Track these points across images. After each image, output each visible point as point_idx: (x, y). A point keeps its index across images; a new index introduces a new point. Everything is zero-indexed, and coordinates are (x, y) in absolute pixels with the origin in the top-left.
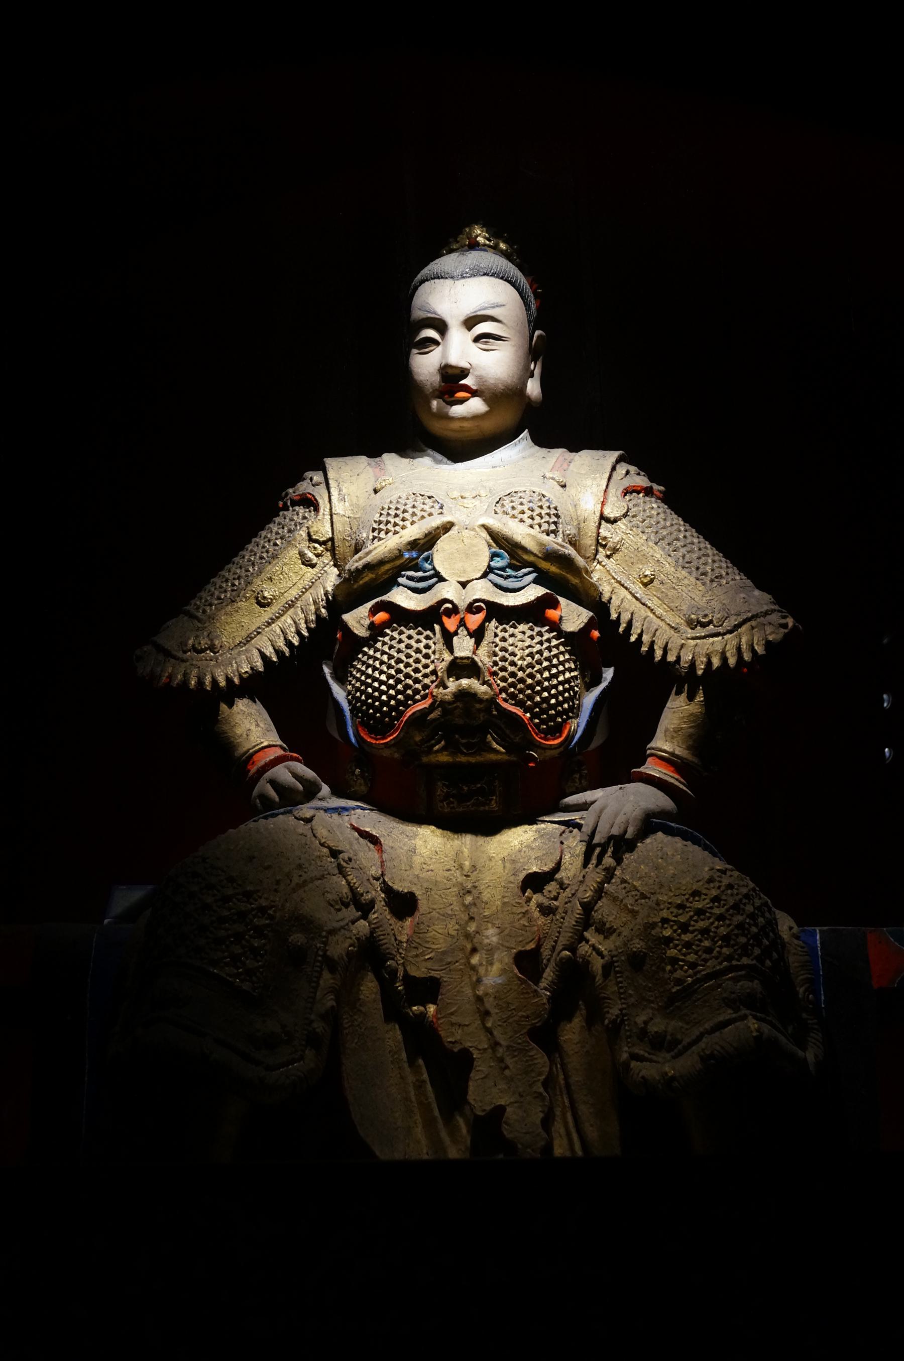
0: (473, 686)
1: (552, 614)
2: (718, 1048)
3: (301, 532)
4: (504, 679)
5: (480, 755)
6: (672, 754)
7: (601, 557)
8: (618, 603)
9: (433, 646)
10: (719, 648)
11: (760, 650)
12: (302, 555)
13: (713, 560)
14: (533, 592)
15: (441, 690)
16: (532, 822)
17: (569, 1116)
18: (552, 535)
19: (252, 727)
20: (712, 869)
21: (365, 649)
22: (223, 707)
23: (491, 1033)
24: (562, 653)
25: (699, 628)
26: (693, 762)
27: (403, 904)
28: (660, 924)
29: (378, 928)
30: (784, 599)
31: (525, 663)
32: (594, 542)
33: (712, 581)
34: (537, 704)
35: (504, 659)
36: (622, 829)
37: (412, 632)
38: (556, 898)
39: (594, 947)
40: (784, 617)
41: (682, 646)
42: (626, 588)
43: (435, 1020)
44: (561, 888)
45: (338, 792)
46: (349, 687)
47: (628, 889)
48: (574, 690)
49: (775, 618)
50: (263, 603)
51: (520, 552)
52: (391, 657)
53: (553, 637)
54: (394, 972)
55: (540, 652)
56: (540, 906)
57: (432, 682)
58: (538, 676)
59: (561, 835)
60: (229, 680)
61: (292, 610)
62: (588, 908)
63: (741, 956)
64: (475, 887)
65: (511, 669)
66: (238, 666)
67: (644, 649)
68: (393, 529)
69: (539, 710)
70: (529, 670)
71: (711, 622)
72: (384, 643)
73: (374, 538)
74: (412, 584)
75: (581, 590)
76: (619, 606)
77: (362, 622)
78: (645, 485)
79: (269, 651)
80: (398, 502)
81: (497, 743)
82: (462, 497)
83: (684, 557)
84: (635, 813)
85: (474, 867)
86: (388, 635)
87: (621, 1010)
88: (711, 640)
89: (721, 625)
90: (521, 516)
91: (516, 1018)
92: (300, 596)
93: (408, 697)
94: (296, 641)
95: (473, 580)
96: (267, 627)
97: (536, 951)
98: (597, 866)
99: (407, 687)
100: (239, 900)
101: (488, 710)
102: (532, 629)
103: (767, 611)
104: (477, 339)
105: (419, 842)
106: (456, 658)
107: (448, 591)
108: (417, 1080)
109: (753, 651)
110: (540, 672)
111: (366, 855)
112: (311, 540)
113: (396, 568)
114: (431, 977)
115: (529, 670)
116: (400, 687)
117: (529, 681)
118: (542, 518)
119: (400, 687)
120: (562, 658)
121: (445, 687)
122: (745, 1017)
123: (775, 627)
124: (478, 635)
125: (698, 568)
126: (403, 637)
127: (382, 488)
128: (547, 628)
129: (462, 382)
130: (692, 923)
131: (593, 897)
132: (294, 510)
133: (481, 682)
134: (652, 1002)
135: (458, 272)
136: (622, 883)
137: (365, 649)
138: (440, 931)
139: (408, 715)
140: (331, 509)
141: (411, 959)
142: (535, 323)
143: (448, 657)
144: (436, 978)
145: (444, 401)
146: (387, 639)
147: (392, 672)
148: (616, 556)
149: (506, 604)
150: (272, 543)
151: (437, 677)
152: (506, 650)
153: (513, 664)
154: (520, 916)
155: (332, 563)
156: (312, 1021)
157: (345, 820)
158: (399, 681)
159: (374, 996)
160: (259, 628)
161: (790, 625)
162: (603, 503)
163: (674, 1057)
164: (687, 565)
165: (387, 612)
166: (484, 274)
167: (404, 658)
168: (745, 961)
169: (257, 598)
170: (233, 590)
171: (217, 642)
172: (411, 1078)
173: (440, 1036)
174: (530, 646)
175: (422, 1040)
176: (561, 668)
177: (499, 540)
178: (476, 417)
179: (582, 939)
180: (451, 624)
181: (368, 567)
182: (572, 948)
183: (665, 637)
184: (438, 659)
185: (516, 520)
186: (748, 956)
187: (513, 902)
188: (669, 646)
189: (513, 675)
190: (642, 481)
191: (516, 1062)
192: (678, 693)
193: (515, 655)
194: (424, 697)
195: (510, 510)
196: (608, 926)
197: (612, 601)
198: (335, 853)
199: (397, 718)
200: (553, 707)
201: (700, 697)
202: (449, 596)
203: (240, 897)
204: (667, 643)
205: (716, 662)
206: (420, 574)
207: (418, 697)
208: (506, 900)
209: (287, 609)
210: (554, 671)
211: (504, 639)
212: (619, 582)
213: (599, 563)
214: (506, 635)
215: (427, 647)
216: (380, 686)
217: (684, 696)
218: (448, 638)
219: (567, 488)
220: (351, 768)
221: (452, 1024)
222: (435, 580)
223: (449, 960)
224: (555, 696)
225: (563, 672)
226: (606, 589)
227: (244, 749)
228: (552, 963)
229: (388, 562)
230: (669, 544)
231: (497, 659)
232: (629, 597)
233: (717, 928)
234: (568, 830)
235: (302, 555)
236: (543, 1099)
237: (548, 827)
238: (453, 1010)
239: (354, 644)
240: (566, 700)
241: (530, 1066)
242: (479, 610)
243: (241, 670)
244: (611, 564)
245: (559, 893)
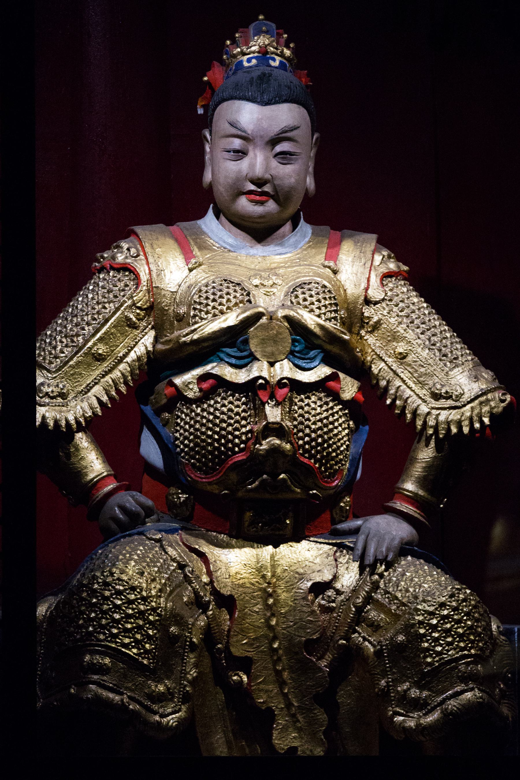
2: (455, 709)
14: (321, 372)
26: (427, 499)
27: (227, 602)
35: (301, 423)
38: (333, 601)
40: (503, 394)
44: (337, 594)
52: (216, 417)
62: (360, 610)
74: (233, 361)
104: (276, 156)
109: (482, 422)
114: (246, 656)
123: (499, 400)
130: (440, 625)
134: (410, 678)
144: (249, 657)
153: (308, 426)
183: (415, 405)
193: (310, 420)
203: (139, 601)
222: (249, 359)
233: (456, 629)
242: (284, 385)
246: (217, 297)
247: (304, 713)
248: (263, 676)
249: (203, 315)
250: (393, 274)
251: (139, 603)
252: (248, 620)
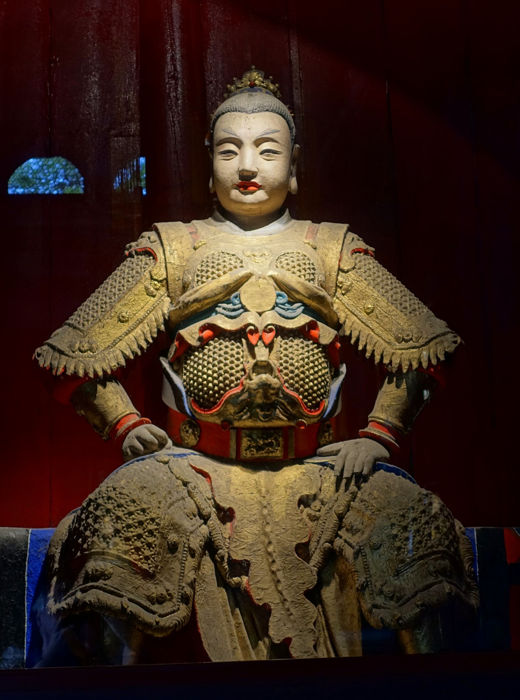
0: (269, 379)
1: (314, 332)
3: (145, 273)
4: (286, 375)
5: (271, 421)
6: (387, 421)
7: (338, 294)
8: (350, 324)
9: (242, 353)
10: (416, 356)
11: (442, 358)
12: (147, 289)
13: (411, 300)
14: (304, 320)
15: (248, 381)
16: (302, 463)
17: (329, 643)
18: (312, 282)
19: (116, 401)
20: (420, 494)
21: (196, 353)
22: (100, 387)
23: (281, 594)
24: (320, 358)
25: (403, 342)
26: (399, 426)
28: (390, 527)
29: (214, 530)
30: (454, 326)
31: (300, 364)
32: (334, 285)
33: (410, 313)
34: (306, 390)
35: (286, 362)
36: (361, 468)
37: (228, 343)
38: (319, 511)
39: (346, 541)
40: (455, 337)
41: (393, 354)
42: (355, 315)
43: (247, 586)
45: (178, 443)
46: (185, 377)
47: (367, 506)
48: (326, 381)
49: (450, 336)
50: (122, 320)
51: (294, 293)
53: (315, 348)
54: (222, 558)
55: (308, 357)
56: (309, 515)
57: (242, 376)
58: (307, 372)
59: (320, 471)
60: (104, 372)
61: (141, 324)
62: (341, 517)
63: (438, 545)
64: (269, 504)
65: (291, 368)
66: (109, 361)
67: (368, 355)
68: (211, 276)
69: (307, 394)
70: (302, 369)
71: (411, 339)
72: (209, 350)
73: (198, 281)
75: (328, 316)
76: (351, 327)
77: (194, 336)
78: (364, 248)
79: (128, 353)
80: (213, 258)
81: (282, 415)
82: (253, 255)
83: (392, 296)
84: (368, 458)
85: (268, 492)
86: (212, 345)
87: (366, 578)
88: (412, 350)
89: (418, 342)
90: (293, 269)
91: (297, 584)
92: (146, 316)
93: (226, 385)
94: (145, 346)
95: (265, 311)
96: (125, 336)
97: (307, 544)
98: (346, 491)
99: (226, 379)
100: (138, 514)
101: (277, 394)
102: (302, 343)
103: (445, 332)
104: (262, 153)
105: (232, 476)
106: (257, 361)
107: (250, 318)
108: (236, 623)
109: (438, 358)
110: (308, 370)
111: (202, 484)
112: (152, 278)
113: (215, 301)
115: (302, 369)
116: (221, 378)
117: (302, 376)
118: (305, 271)
119: (221, 378)
120: (320, 361)
121: (251, 379)
122: (441, 581)
123: (450, 342)
124: (270, 346)
125: (401, 304)
126: (222, 346)
127: (200, 246)
128: (311, 342)
129: (253, 180)
131: (344, 510)
132: (138, 258)
133: (273, 376)
135: (250, 108)
136: (362, 501)
137: (196, 353)
138: (249, 531)
139: (227, 396)
140: (165, 259)
141: (233, 549)
142: (295, 141)
143: (252, 362)
145: (240, 191)
146: (211, 347)
147: (216, 369)
148: (349, 294)
149: (287, 327)
150: (125, 280)
151: (245, 373)
152: (287, 356)
153: (292, 365)
154: (298, 522)
155: (166, 294)
156: (184, 587)
157: (184, 462)
158: (221, 375)
159: (211, 572)
160: (120, 336)
161: (459, 341)
162: (340, 261)
163: (400, 606)
164: (394, 302)
165: (211, 330)
166: (267, 110)
167: (223, 360)
168: (441, 548)
169: (119, 317)
170: (102, 311)
171: (94, 346)
172: (233, 622)
173: (251, 595)
174: (302, 354)
175: (239, 598)
176: (320, 367)
177: (282, 286)
178: (261, 203)
179: (337, 535)
180: (253, 339)
181: (196, 300)
182: (331, 542)
183: (382, 347)
184: (245, 361)
185: (290, 272)
186: (442, 545)
187: (293, 513)
188: (385, 354)
189: (292, 372)
190: (361, 244)
191: (297, 611)
192: (390, 382)
194: (236, 385)
195: (285, 266)
196: (355, 528)
197: (346, 323)
198: (185, 484)
199: (219, 398)
200: (314, 392)
201: (404, 386)
202: (251, 321)
203: (139, 512)
204: (383, 352)
205: (415, 365)
206: (230, 306)
207: (232, 385)
208: (288, 512)
209: (138, 325)
210: (316, 369)
211: (286, 349)
212: (351, 312)
213: (338, 298)
214: (287, 346)
215: (238, 353)
216: (208, 377)
217: (394, 384)
218: (251, 348)
219: (317, 250)
220: (185, 428)
221: (258, 588)
222: (242, 310)
223: (255, 549)
224: (316, 385)
225: (321, 370)
226: (342, 316)
227: (115, 416)
228: (318, 551)
229: (210, 298)
230: (382, 288)
231: (282, 361)
232: (358, 321)
234: (323, 468)
235: (147, 289)
236: (315, 633)
237: (310, 466)
238: (258, 579)
239: (187, 350)
240: (322, 387)
241: (306, 613)
242: (271, 330)
243: (111, 364)
244: (345, 299)
245: (321, 508)
246: (215, 265)
247: (297, 607)
248: (260, 576)
249: (204, 279)
250: (361, 250)
251: (138, 514)
252: (246, 529)
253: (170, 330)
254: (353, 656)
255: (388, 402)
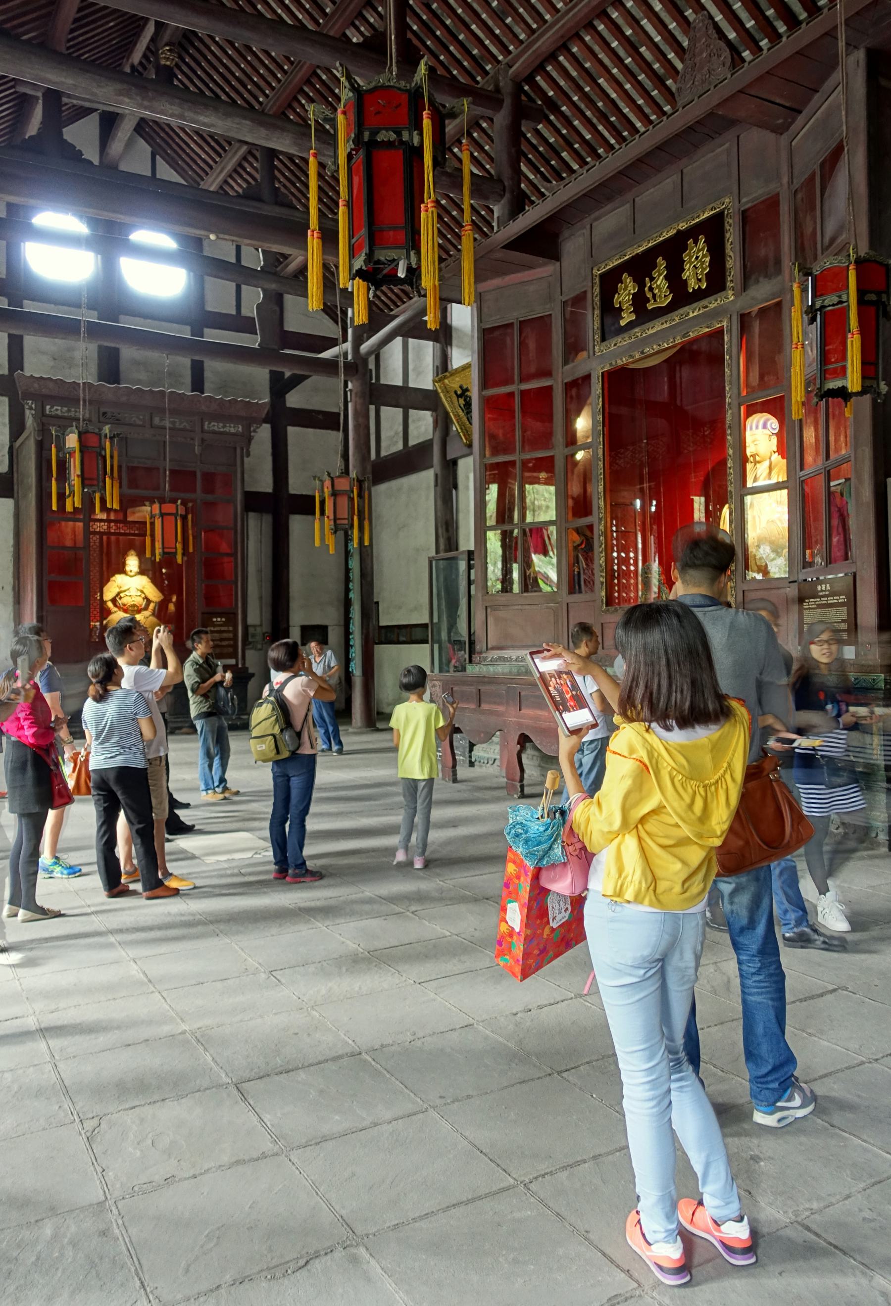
19: (110, 605)
253: (118, 594)
254: (307, 835)
255: (152, 606)
